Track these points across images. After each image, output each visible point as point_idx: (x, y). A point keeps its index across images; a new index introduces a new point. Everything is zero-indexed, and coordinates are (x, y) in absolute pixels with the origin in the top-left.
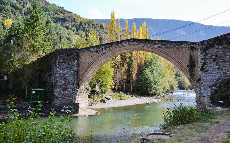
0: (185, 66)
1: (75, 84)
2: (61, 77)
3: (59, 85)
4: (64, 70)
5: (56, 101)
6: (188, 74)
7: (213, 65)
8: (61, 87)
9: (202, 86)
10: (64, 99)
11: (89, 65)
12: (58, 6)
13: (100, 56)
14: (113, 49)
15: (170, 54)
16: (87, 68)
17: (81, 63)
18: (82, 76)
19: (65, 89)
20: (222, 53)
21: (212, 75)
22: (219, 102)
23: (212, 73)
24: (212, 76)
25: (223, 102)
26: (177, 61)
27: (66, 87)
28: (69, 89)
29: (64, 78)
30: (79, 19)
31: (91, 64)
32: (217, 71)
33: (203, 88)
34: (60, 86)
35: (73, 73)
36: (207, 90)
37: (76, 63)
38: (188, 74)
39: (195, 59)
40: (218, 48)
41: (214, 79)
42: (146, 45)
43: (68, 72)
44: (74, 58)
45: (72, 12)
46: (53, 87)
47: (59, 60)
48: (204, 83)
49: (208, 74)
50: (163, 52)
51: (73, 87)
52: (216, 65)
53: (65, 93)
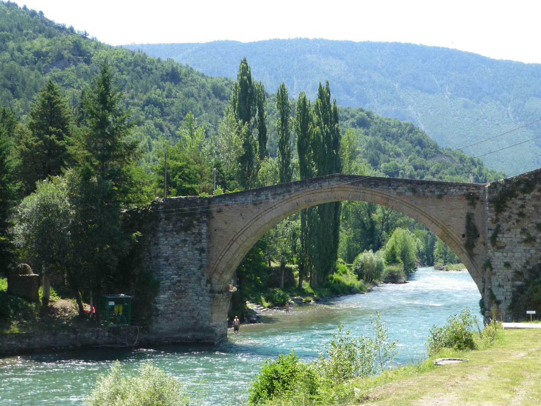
0: (456, 237)
1: (203, 282)
2: (170, 264)
3: (166, 284)
4: (176, 249)
5: (159, 321)
6: (464, 254)
7: (516, 235)
8: (169, 290)
9: (493, 278)
10: (179, 316)
11: (237, 236)
12: (25, 8)
13: (263, 214)
14: (293, 198)
15: (423, 210)
16: (231, 243)
17: (215, 230)
18: (218, 262)
19: (181, 293)
20: (533, 208)
21: (513, 256)
22: (528, 312)
23: (514, 250)
24: (513, 258)
25: (534, 312)
26: (439, 225)
27: (183, 289)
28: (190, 294)
29: (178, 268)
30: (102, 53)
31: (242, 231)
32: (523, 247)
33: (497, 284)
34: (169, 286)
35: (198, 255)
36: (505, 287)
37: (205, 231)
38: (464, 254)
39: (478, 222)
40: (523, 199)
41: (517, 264)
42: (369, 189)
43: (185, 253)
44: (198, 220)
45: (72, 29)
46: (155, 288)
47: (165, 226)
48: (498, 274)
49: (505, 254)
50: (408, 205)
51: (199, 289)
52: (521, 233)
53: (181, 304)
